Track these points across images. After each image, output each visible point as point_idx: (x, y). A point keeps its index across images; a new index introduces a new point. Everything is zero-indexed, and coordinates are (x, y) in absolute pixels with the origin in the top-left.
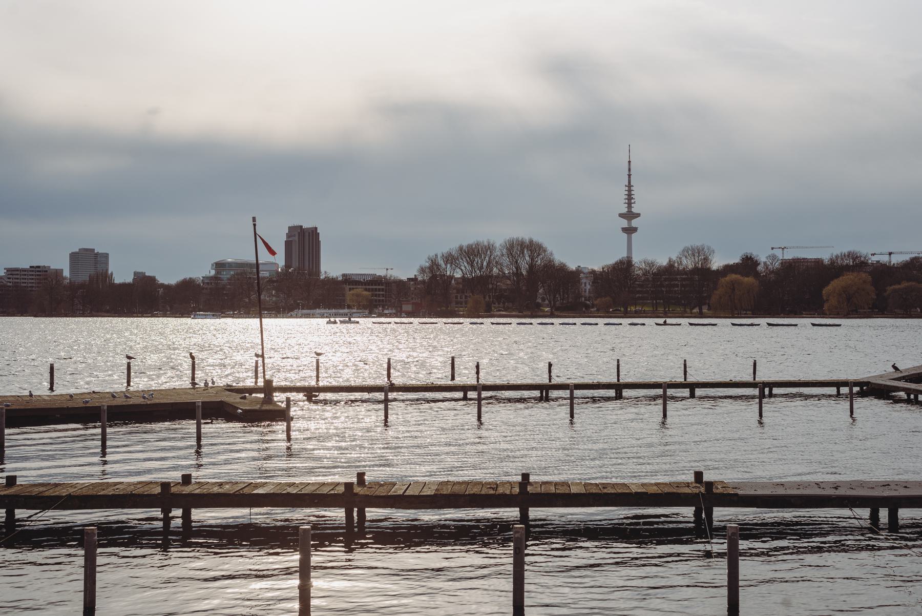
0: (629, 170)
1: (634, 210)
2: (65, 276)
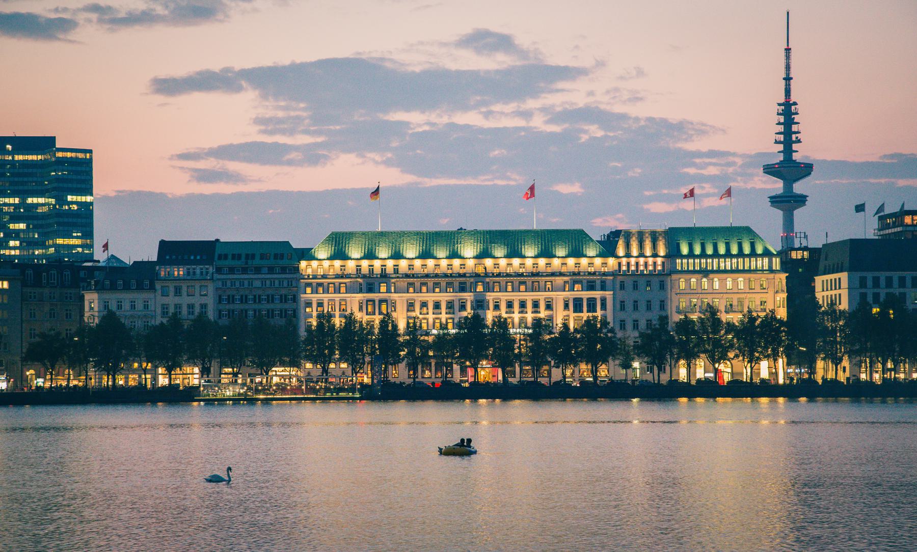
0: (788, 67)
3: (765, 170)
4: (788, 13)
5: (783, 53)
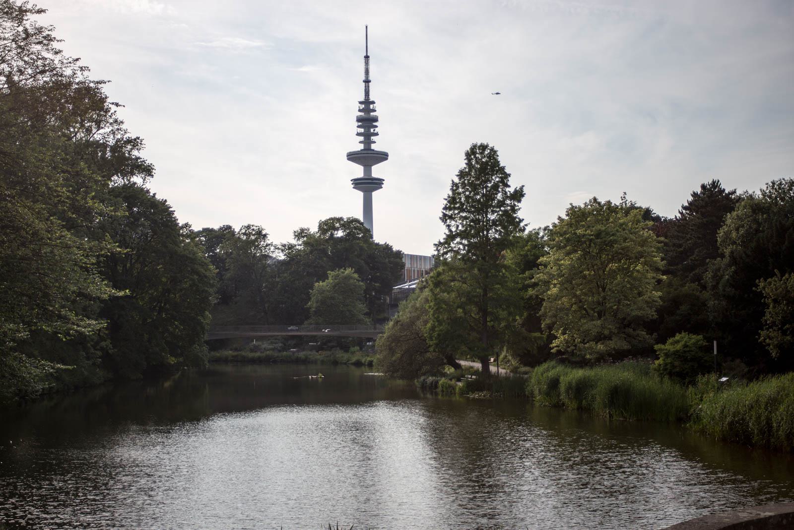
0: (367, 72)
1: (378, 146)
2: (113, 470)
3: (349, 157)
4: (367, 27)
5: (363, 60)
